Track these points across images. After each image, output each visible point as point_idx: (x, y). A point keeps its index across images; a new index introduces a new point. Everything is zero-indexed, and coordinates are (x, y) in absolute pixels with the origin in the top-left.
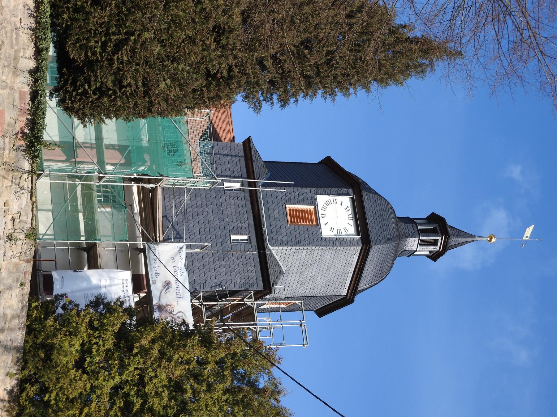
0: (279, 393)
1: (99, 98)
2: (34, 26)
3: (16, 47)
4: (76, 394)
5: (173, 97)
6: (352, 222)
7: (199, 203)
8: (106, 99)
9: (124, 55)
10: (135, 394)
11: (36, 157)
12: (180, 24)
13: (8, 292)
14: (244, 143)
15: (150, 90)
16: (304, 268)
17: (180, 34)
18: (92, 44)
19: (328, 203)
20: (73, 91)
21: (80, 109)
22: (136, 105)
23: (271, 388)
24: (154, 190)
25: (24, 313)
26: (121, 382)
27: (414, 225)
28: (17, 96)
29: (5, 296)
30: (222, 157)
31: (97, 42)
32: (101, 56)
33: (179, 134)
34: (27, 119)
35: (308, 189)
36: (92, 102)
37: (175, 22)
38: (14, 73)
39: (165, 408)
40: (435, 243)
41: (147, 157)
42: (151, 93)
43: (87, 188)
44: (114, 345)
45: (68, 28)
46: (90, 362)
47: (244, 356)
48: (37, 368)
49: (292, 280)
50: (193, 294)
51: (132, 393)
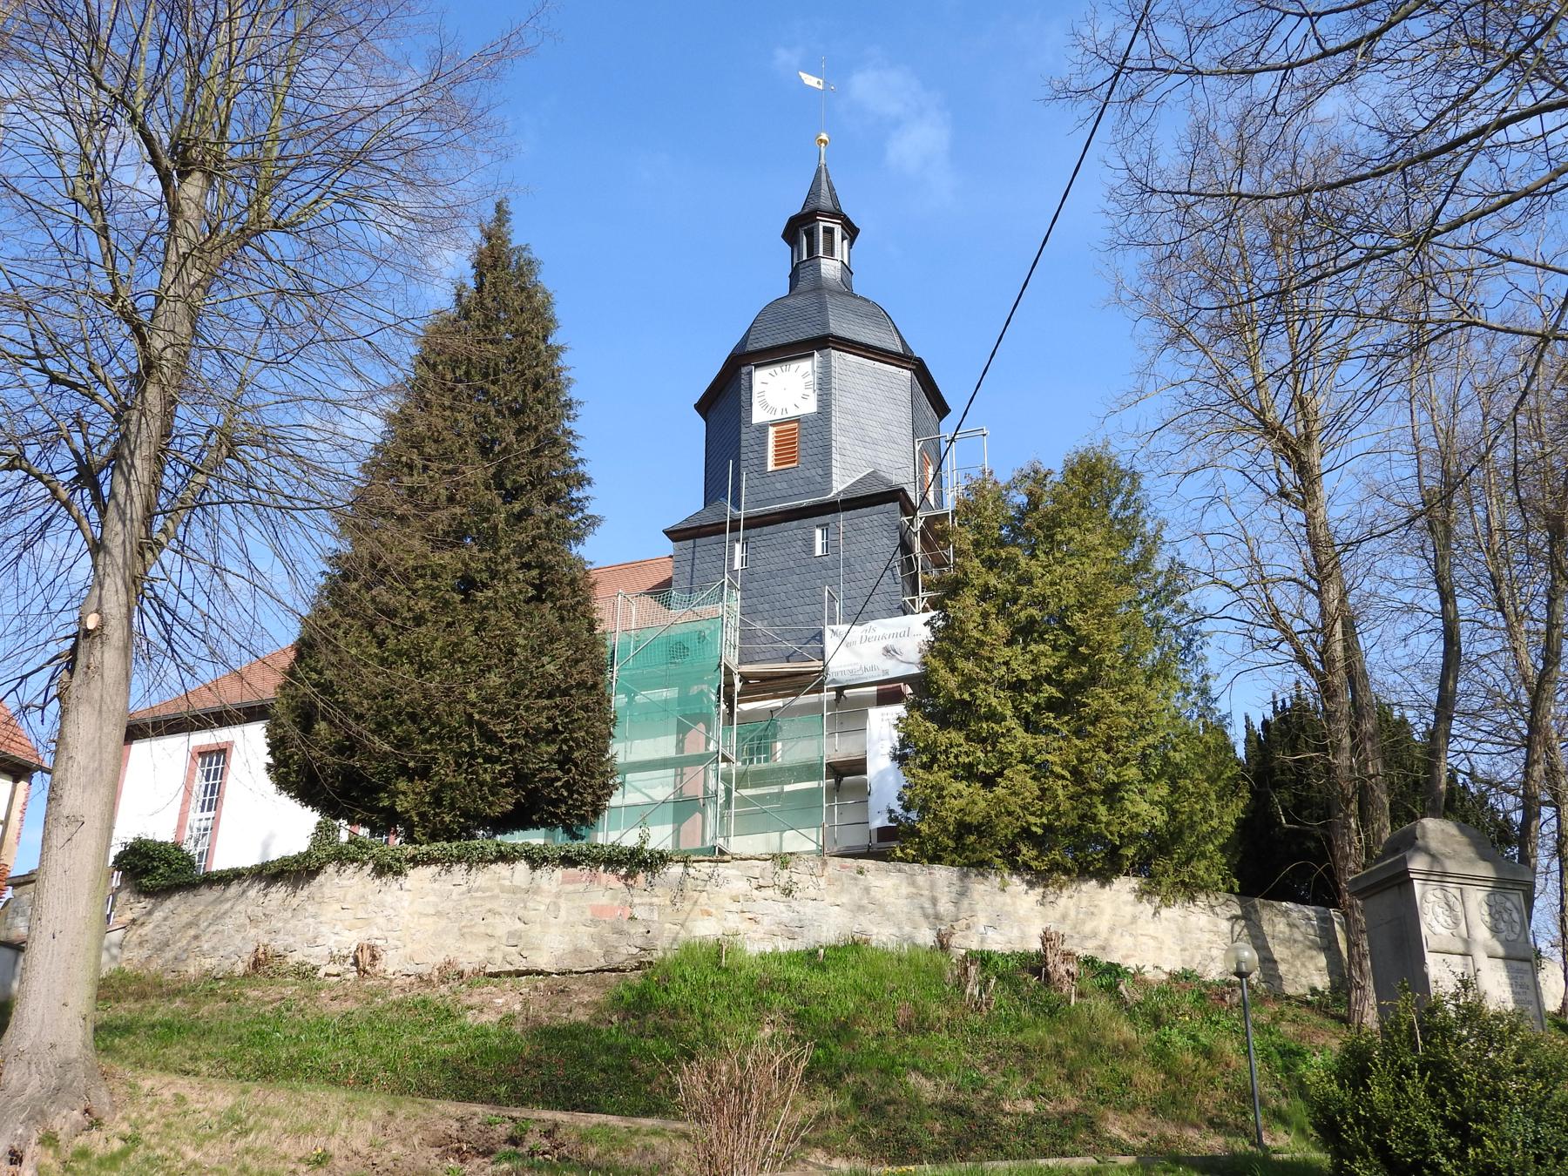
0: (1036, 472)
1: (576, 766)
2: (464, 866)
3: (497, 891)
4: (1033, 786)
5: (571, 652)
6: (794, 366)
7: (766, 606)
8: (576, 754)
9: (504, 728)
10: (1035, 694)
11: (662, 856)
12: (456, 645)
13: (872, 893)
14: (674, 540)
15: (558, 686)
16: (867, 439)
17: (471, 644)
18: (488, 778)
19: (765, 405)
20: (566, 803)
21: (594, 793)
22: (585, 708)
23: (1028, 484)
24: (745, 678)
25: (906, 867)
26: (1018, 718)
27: (801, 266)
28: (570, 888)
29: (879, 896)
30: (696, 574)
31: (485, 770)
32: (506, 762)
33: (656, 642)
34: (605, 871)
35: (743, 437)
36: (582, 774)
37: (452, 652)
38: (535, 893)
39: (1055, 648)
40: (829, 232)
41: (695, 690)
42: (563, 686)
43: (743, 780)
44: (961, 730)
45: (465, 814)
46: (986, 765)
47: (979, 528)
48: (992, 846)
49: (886, 456)
50: (905, 610)
51: (1034, 699)
